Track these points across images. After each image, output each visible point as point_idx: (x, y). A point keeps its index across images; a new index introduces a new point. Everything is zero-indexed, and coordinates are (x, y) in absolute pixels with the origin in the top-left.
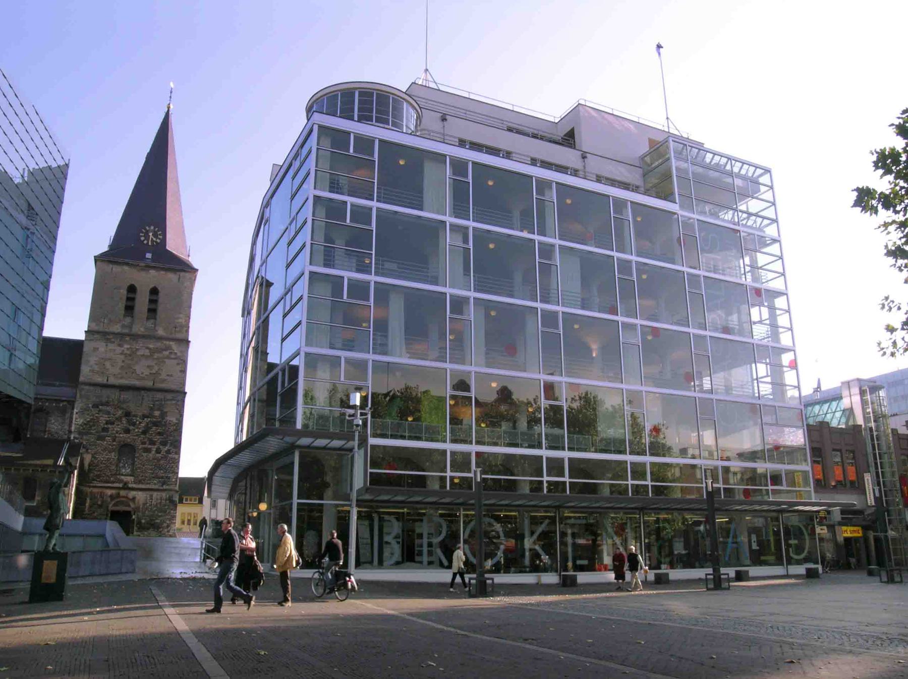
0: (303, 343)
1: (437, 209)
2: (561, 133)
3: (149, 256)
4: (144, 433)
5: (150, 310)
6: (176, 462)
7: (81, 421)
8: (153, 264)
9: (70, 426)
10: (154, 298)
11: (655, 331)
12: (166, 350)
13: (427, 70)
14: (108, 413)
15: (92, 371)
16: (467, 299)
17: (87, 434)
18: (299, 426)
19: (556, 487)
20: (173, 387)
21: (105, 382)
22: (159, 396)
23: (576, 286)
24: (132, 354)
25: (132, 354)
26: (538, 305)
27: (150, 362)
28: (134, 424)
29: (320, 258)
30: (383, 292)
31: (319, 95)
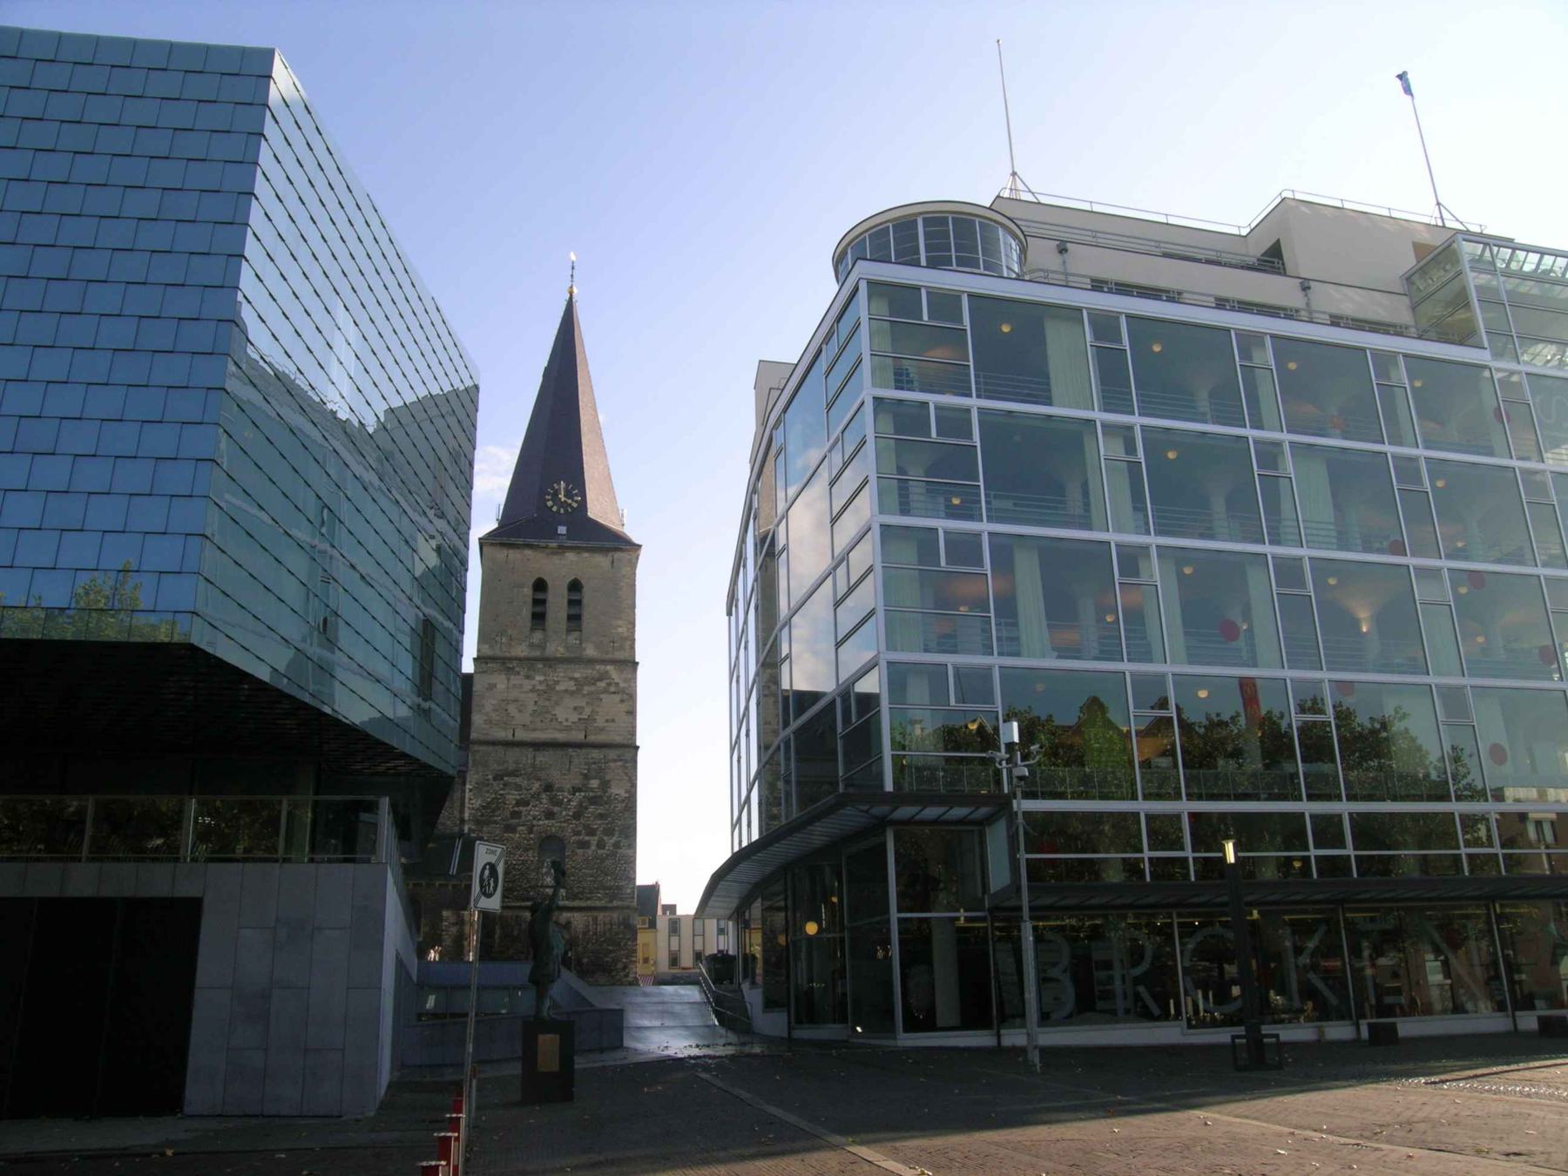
0: (883, 647)
1: (1074, 400)
2: (1256, 251)
3: (562, 530)
4: (577, 816)
5: (571, 618)
6: (631, 862)
7: (478, 803)
8: (569, 543)
9: (462, 812)
10: (575, 597)
11: (1476, 578)
12: (600, 680)
13: (1014, 174)
14: (518, 787)
15: (489, 722)
16: (1145, 549)
17: (488, 823)
18: (889, 786)
19: (1333, 866)
20: (618, 739)
21: (510, 737)
22: (596, 754)
23: (1324, 511)
24: (549, 690)
25: (550, 689)
26: (1267, 549)
27: (581, 702)
28: (560, 803)
29: (894, 500)
30: (1004, 549)
31: (859, 230)
